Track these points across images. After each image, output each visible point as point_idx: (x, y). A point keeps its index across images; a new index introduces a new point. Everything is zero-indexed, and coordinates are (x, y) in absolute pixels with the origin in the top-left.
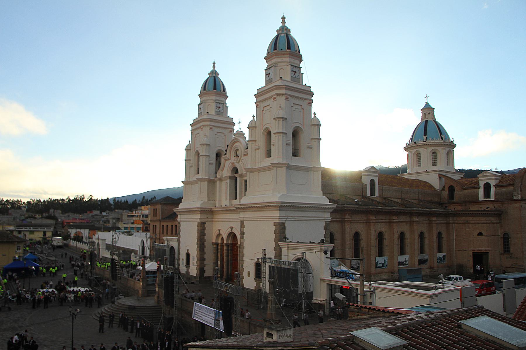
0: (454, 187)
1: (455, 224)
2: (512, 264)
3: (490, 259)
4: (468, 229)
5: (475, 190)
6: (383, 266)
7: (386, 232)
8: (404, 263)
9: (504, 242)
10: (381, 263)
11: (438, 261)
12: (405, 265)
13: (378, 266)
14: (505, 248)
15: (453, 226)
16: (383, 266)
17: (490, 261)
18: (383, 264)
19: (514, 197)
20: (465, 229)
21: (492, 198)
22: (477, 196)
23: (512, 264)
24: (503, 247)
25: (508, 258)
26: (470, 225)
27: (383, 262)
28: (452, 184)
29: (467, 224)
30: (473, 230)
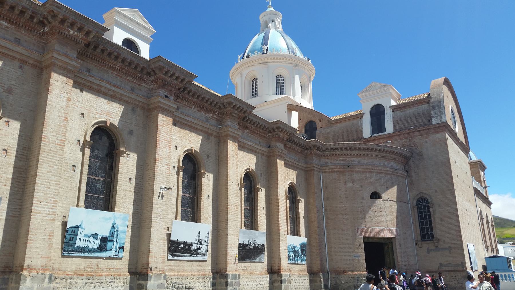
0: (315, 123)
1: (324, 174)
2: (441, 264)
3: (398, 254)
4: (350, 185)
5: (355, 122)
6: (102, 248)
7: (131, 132)
8: (194, 247)
9: (421, 217)
10: (95, 236)
11: (289, 256)
12: (197, 254)
13: (78, 244)
14: (422, 230)
15: (319, 179)
16: (102, 248)
17: (399, 259)
18: (104, 240)
19: (433, 120)
20: (345, 184)
21: (389, 128)
22: (359, 130)
23: (441, 264)
24: (418, 228)
25: (431, 250)
26: (355, 175)
27: (107, 234)
28: (311, 118)
29: (347, 174)
30: (361, 187)
